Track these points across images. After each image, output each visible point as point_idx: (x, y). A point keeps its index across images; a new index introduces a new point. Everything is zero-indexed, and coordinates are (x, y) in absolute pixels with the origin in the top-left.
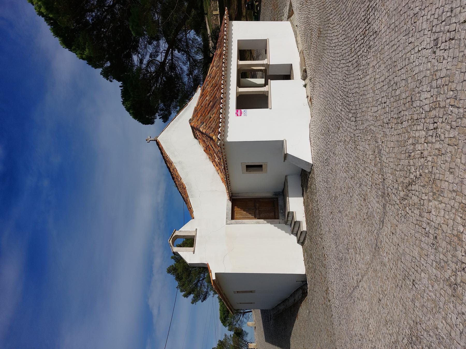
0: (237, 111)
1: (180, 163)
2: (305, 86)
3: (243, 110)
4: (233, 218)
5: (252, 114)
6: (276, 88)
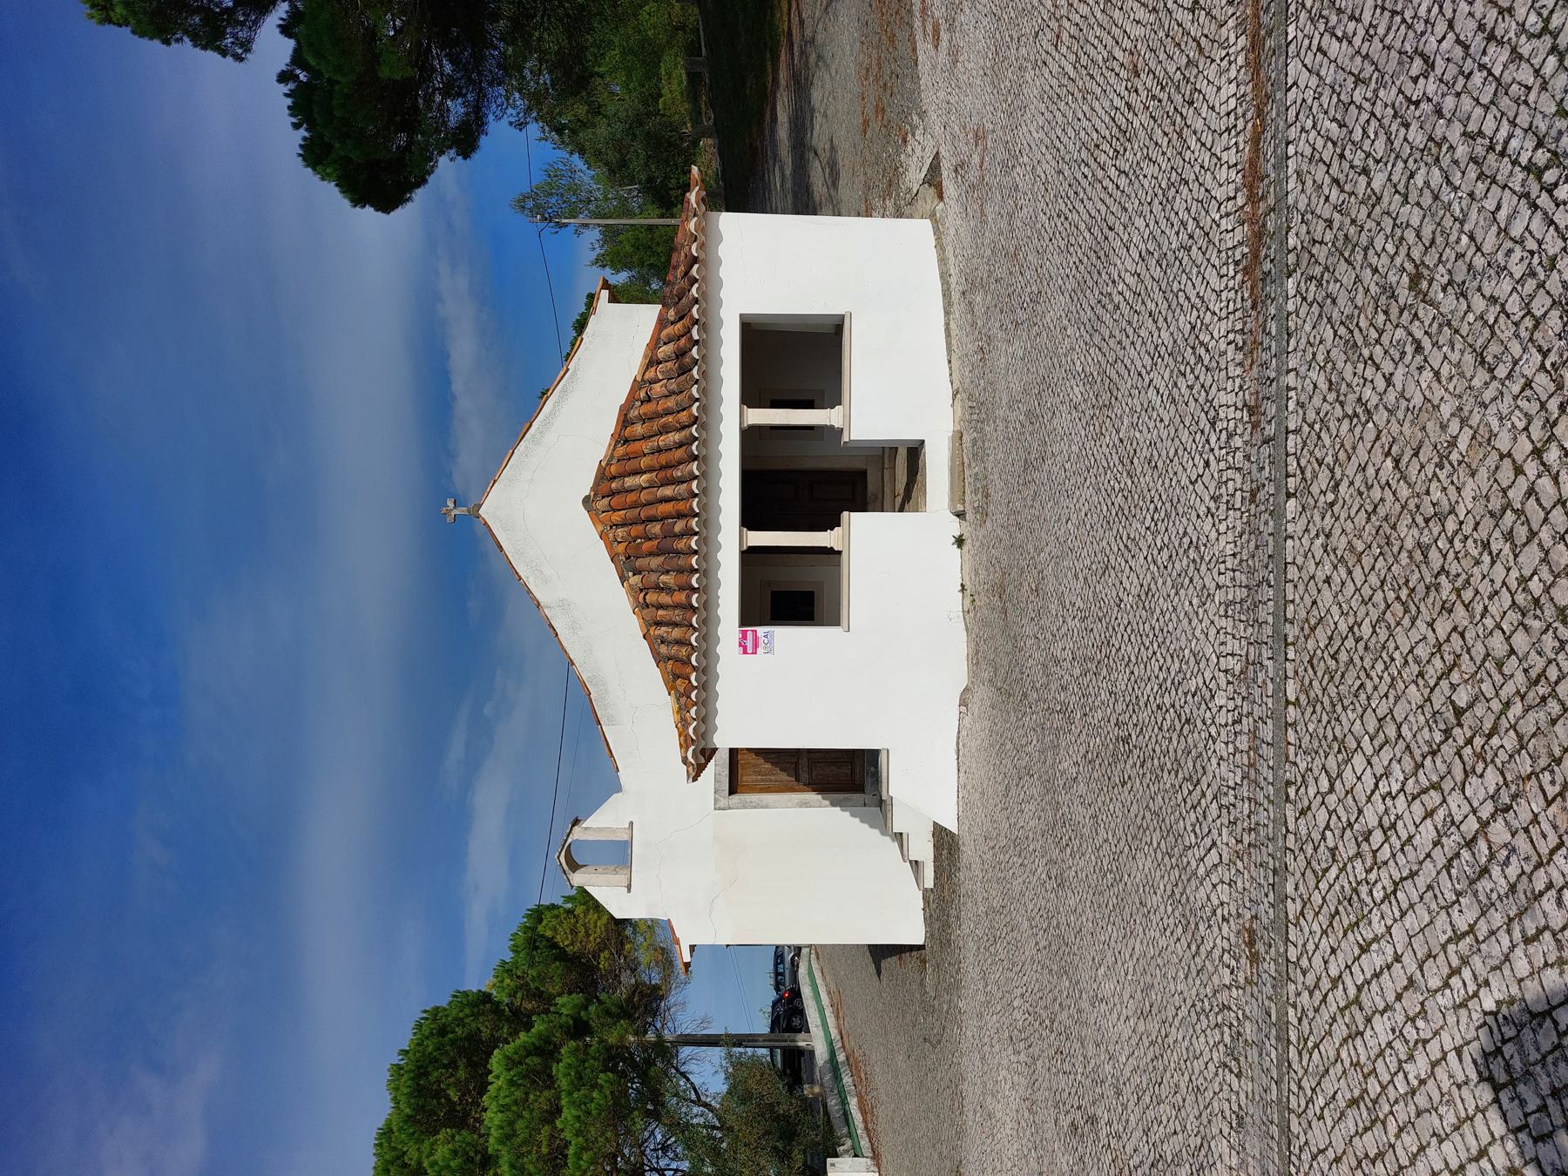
0: (744, 634)
1: (564, 605)
2: (960, 542)
3: (761, 630)
4: (732, 791)
5: (789, 641)
6: (865, 538)
